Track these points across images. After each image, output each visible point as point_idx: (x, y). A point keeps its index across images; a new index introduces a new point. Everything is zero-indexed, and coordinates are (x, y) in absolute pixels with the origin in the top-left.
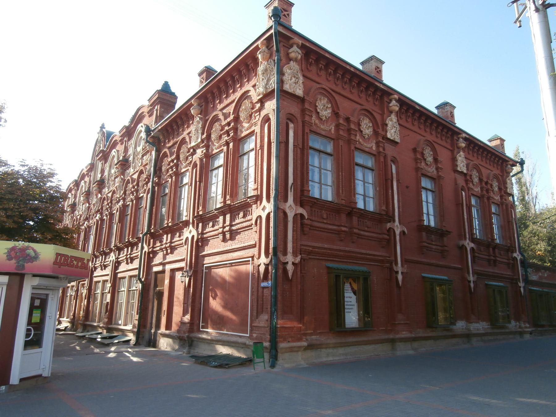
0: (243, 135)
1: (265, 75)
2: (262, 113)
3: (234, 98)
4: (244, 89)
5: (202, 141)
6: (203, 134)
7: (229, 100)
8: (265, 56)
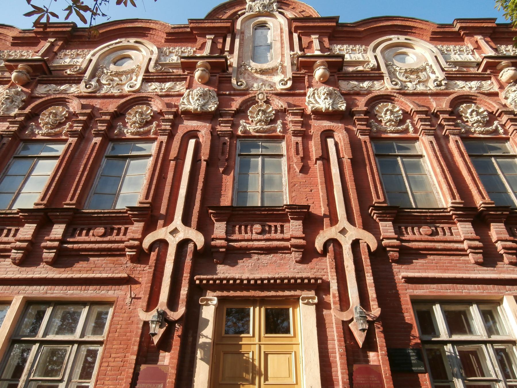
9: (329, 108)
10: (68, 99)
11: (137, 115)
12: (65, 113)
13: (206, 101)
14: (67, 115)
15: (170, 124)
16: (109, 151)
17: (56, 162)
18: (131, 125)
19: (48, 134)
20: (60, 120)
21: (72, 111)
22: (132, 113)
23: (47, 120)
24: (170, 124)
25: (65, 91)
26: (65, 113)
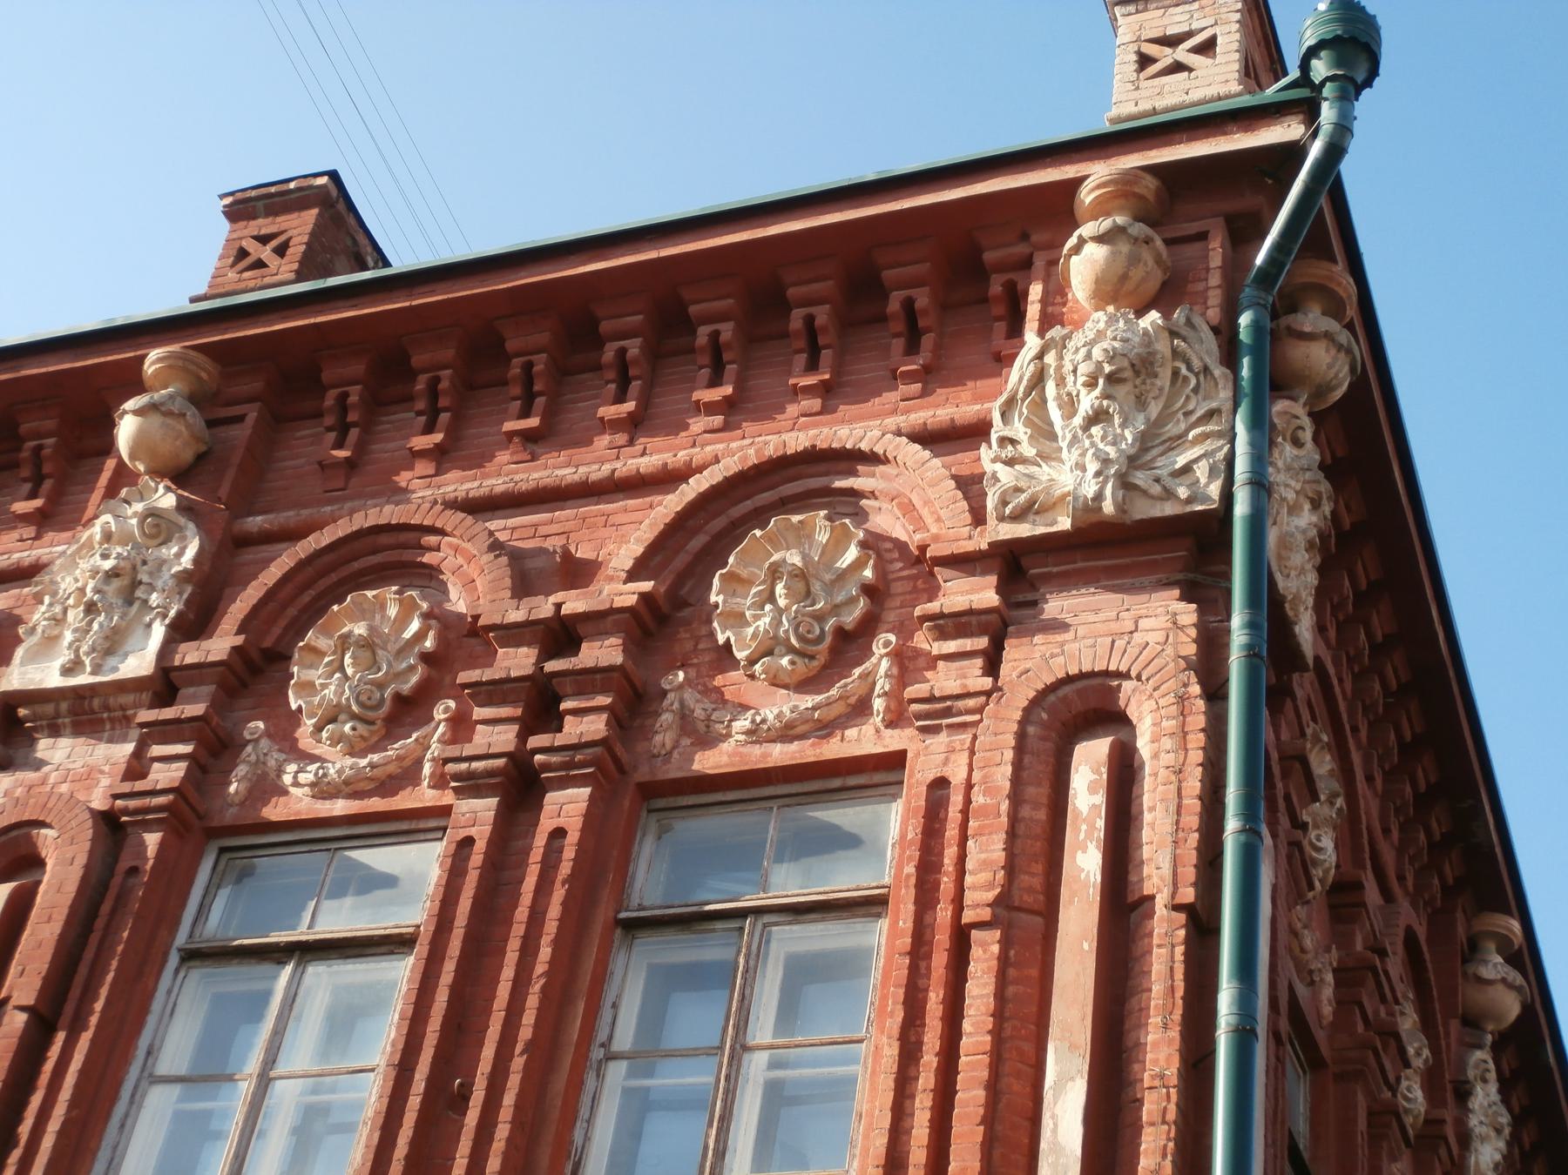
0: (709, 762)
1: (1122, 391)
2: (1016, 655)
3: (698, 455)
4: (843, 432)
5: (166, 683)
6: (191, 626)
7: (650, 457)
8: (1137, 274)
9: (1099, 497)
10: (433, 530)
11: (780, 589)
12: (415, 625)
13: (1154, 409)
14: (429, 644)
15: (185, 749)
16: (650, 884)
17: (402, 971)
18: (319, 729)
19: (351, 788)
20: (836, 609)
21: (461, 607)
22: (323, 643)
23: (330, 692)
24: (185, 749)
25: (1201, 300)
26: (415, 625)
